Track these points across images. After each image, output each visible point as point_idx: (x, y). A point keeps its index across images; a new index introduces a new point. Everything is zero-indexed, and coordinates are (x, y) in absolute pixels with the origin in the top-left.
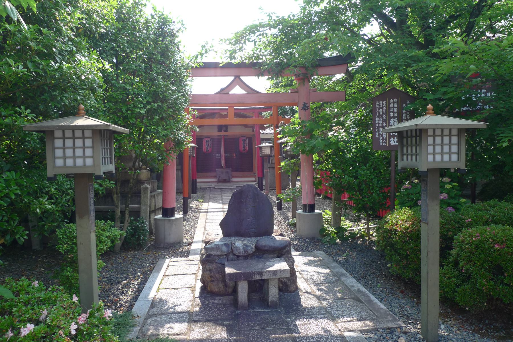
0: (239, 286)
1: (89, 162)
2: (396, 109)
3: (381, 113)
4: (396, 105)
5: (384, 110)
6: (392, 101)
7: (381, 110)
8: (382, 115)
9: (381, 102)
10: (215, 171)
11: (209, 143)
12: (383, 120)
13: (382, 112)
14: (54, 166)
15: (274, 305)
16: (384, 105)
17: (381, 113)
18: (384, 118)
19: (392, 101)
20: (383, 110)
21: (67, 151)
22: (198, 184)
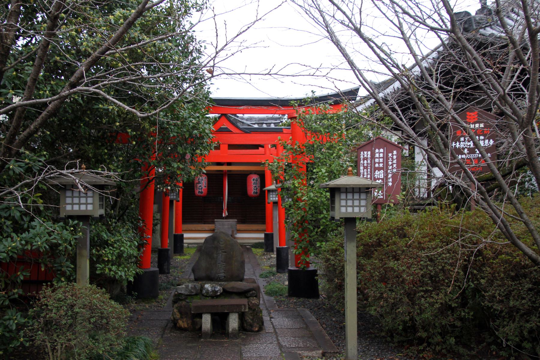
0: (210, 324)
1: (90, 207)
2: (381, 160)
3: (365, 165)
4: (381, 155)
5: (369, 162)
6: (377, 151)
7: (365, 162)
8: (367, 167)
9: (365, 153)
10: (213, 222)
11: (518, 109)
12: (367, 172)
13: (367, 163)
14: (340, 212)
15: (235, 335)
16: (369, 156)
17: (365, 165)
18: (369, 170)
19: (377, 151)
20: (367, 161)
21: (85, 206)
22: (185, 241)
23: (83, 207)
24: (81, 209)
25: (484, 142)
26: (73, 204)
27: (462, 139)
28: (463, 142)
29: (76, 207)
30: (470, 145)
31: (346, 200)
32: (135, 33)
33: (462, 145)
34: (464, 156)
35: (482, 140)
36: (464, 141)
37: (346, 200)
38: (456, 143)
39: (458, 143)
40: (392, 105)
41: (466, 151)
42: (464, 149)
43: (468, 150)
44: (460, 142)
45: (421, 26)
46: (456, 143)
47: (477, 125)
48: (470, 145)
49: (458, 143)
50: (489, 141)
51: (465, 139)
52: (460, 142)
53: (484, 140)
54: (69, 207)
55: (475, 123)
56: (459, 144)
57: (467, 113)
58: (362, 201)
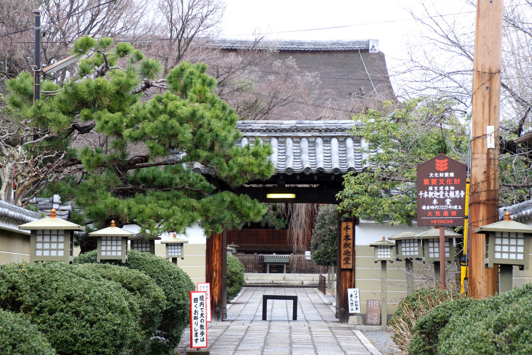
1: (119, 254)
23: (114, 254)
24: (522, 251)
25: (455, 194)
26: (106, 251)
27: (431, 188)
28: (431, 191)
29: (109, 254)
30: (439, 196)
31: (434, 247)
32: (19, 45)
33: (431, 194)
34: (432, 207)
35: (452, 191)
36: (433, 190)
37: (434, 247)
38: (423, 192)
39: (426, 193)
40: (39, 13)
41: (435, 202)
42: (432, 199)
43: (446, 203)
44: (428, 191)
45: (444, 89)
46: (423, 192)
47: (447, 175)
48: (439, 196)
49: (426, 193)
50: (460, 192)
51: (434, 189)
52: (428, 191)
53: (454, 191)
54: (103, 254)
55: (444, 172)
56: (428, 194)
57: (437, 160)
58: (435, 249)
